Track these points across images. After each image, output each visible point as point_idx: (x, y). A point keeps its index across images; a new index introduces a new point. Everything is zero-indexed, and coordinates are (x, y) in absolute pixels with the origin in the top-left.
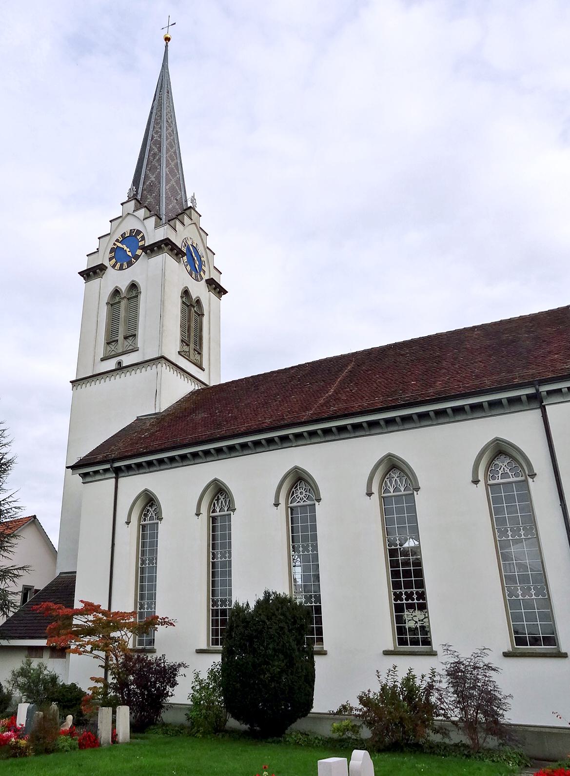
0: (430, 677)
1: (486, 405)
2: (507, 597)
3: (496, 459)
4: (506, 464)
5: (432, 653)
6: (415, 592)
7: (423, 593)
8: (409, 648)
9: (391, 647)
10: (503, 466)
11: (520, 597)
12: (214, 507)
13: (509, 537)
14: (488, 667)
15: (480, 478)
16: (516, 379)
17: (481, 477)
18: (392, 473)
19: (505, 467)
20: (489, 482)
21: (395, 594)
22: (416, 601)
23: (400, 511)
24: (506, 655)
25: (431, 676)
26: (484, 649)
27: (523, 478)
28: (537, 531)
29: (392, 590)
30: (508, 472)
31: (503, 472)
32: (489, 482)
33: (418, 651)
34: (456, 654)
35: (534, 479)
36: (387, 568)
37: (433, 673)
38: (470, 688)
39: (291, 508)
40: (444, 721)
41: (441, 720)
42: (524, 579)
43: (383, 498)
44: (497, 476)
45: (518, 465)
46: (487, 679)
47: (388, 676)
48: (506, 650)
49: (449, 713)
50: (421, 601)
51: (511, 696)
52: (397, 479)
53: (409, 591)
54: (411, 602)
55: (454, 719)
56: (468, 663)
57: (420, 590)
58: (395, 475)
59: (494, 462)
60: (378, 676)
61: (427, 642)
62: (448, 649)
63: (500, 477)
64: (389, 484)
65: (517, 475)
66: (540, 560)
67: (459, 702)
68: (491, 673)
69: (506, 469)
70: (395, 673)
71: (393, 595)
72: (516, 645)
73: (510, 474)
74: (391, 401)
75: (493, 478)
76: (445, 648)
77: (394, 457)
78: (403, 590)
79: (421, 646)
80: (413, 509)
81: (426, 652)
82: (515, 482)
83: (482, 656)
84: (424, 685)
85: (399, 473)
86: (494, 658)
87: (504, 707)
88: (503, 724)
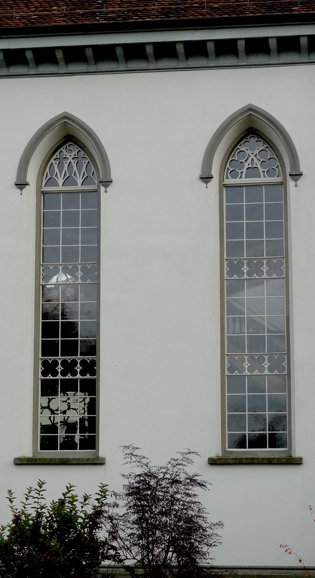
0: (97, 499)
1: (273, 44)
2: (226, 371)
3: (242, 142)
4: (256, 152)
5: (97, 462)
6: (79, 361)
7: (94, 363)
8: (58, 453)
9: (28, 453)
10: (252, 156)
11: (246, 372)
12: (52, 174)
13: (77, 280)
14: (192, 481)
15: (302, 169)
16: (296, 5)
17: (215, 171)
18: (64, 151)
19: (254, 158)
20: (225, 180)
21: (45, 363)
22: (79, 376)
23: (71, 219)
24: (213, 462)
25: (99, 497)
26: (187, 454)
27: (280, 179)
28: (287, 267)
29: (40, 357)
30: (259, 166)
31: (250, 166)
32: (227, 182)
33: (74, 459)
34: (144, 461)
35: (298, 182)
36: (36, 318)
37: (103, 492)
38: (162, 513)
39: (281, 184)
40: (114, 567)
41: (109, 567)
42: (256, 344)
43: (44, 193)
44: (240, 172)
45: (275, 157)
46: (188, 499)
47: (27, 499)
48: (213, 455)
49: (123, 554)
50: (88, 376)
51: (220, 524)
52: (72, 161)
53: (69, 358)
54: (71, 377)
55: (128, 563)
56: (161, 476)
57: (88, 358)
58: (70, 153)
59: (238, 147)
60: (10, 500)
61: (90, 443)
62: (132, 454)
63: (244, 174)
64: (56, 170)
65: (270, 173)
66: (285, 315)
67: (140, 537)
68: (196, 490)
69: (256, 161)
70: (41, 493)
71: (40, 366)
72: (229, 448)
73: (261, 170)
74: (82, 15)
75: (234, 174)
76: (128, 451)
77: (73, 121)
78: (60, 357)
79: (59, 450)
80: (94, 219)
81: (88, 459)
82: (268, 185)
83: (184, 463)
84: (90, 510)
85: (77, 151)
86: (198, 467)
87: (211, 541)
88: (204, 567)
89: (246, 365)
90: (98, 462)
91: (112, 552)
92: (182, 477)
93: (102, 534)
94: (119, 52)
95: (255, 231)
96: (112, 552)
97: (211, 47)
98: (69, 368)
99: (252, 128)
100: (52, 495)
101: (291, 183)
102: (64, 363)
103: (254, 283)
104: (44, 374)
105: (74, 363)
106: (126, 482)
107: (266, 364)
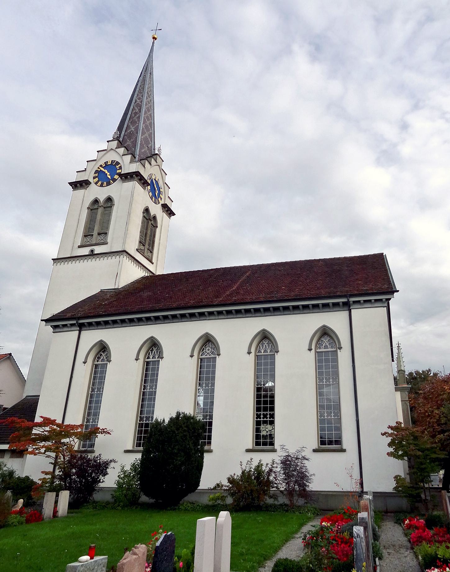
9: (250, 447)
11: (326, 417)
14: (304, 458)
17: (313, 347)
21: (257, 414)
23: (266, 364)
24: (315, 451)
27: (335, 349)
32: (317, 350)
38: (293, 471)
42: (329, 407)
43: (318, 352)
48: (314, 448)
51: (314, 475)
53: (265, 413)
58: (266, 343)
61: (272, 444)
68: (305, 461)
80: (273, 364)
82: (331, 351)
86: (308, 453)
89: (326, 415)
90: (274, 451)
91: (275, 485)
92: (300, 457)
93: (271, 478)
94: (252, 310)
95: (327, 367)
96: (275, 485)
97: (311, 306)
98: (265, 416)
99: (325, 333)
100: (255, 464)
101: (339, 351)
102: (263, 414)
103: (328, 386)
104: (257, 418)
105: (267, 414)
106: (280, 458)
107: (333, 414)
